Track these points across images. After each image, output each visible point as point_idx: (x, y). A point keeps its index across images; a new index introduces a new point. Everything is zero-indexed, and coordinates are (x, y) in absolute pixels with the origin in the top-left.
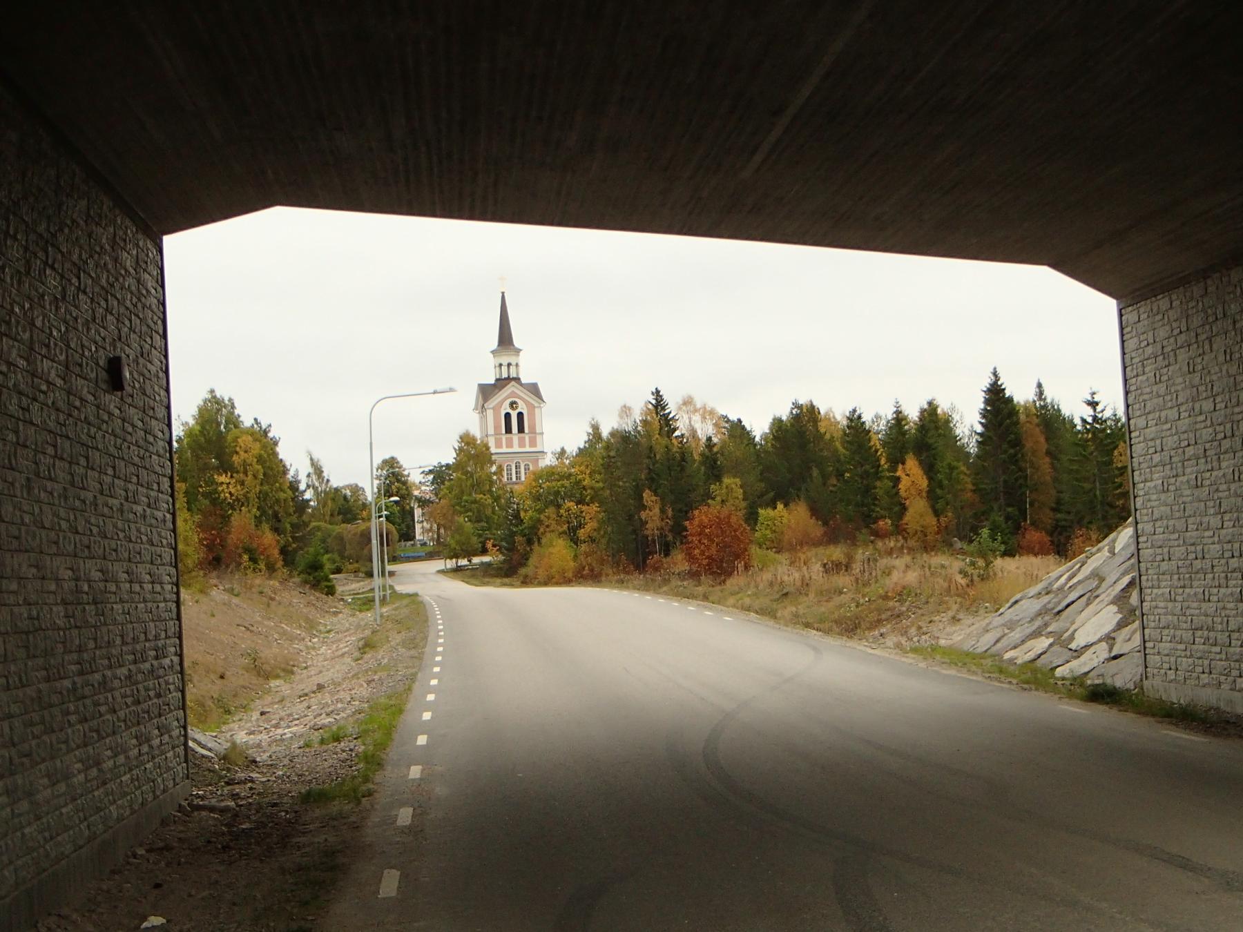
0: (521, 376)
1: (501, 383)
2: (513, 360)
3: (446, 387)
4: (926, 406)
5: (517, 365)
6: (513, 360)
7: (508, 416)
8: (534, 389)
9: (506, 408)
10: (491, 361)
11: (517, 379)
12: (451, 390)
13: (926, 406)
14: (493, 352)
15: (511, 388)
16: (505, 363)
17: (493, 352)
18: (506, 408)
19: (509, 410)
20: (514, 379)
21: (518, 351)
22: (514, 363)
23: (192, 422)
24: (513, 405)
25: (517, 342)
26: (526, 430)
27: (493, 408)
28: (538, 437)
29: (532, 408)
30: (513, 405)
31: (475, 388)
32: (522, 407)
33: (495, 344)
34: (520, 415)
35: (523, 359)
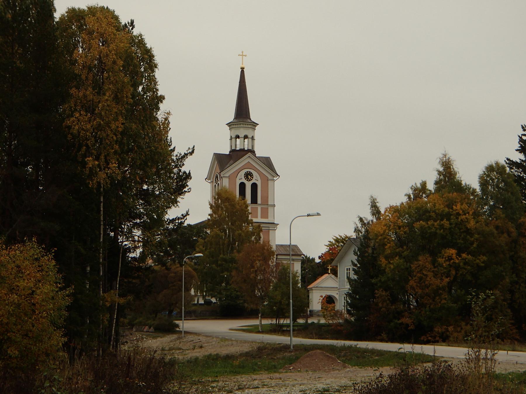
0: (256, 150)
1: (236, 154)
2: (249, 133)
3: (315, 212)
4: (419, 185)
5: (253, 138)
6: (249, 133)
7: (242, 186)
8: (267, 162)
9: (241, 178)
10: (227, 133)
11: (252, 152)
12: (318, 214)
13: (419, 185)
14: (229, 124)
15: (245, 160)
16: (242, 135)
17: (229, 124)
18: (241, 178)
19: (244, 180)
20: (249, 151)
21: (255, 125)
22: (250, 136)
23: (470, 176)
24: (248, 176)
25: (254, 117)
26: (259, 201)
27: (229, 177)
28: (270, 209)
29: (266, 181)
30: (248, 176)
31: (211, 156)
32: (257, 179)
33: (231, 116)
34: (254, 187)
35: (258, 133)
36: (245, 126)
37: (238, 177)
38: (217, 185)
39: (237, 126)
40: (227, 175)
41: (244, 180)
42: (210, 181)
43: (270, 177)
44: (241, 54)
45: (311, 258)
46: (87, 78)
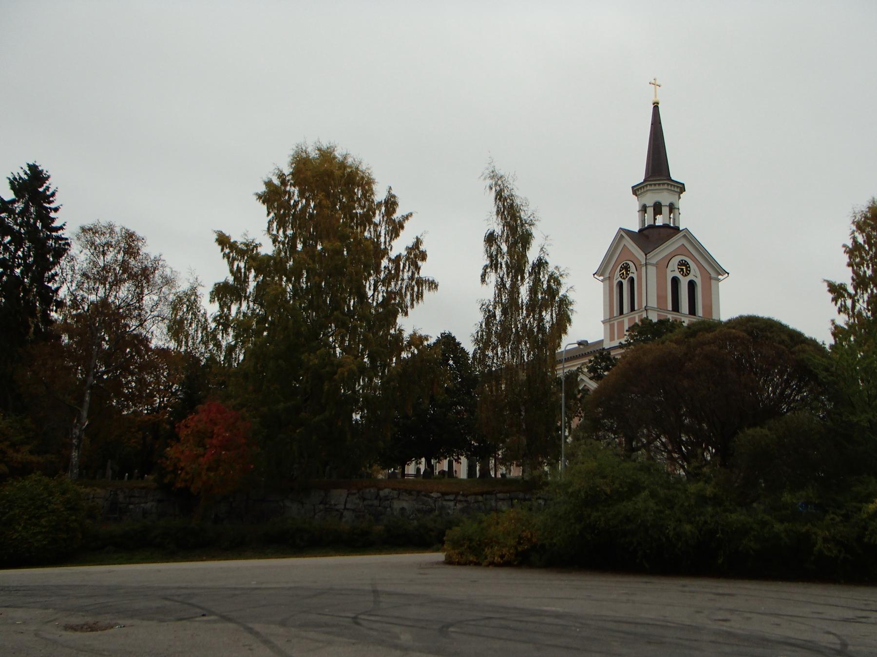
7: (675, 281)
9: (673, 270)
10: (634, 204)
18: (673, 270)
21: (681, 188)
24: (684, 267)
26: (636, 308)
27: (657, 265)
30: (684, 267)
33: (640, 177)
34: (692, 285)
35: (684, 202)
36: (653, 187)
38: (625, 283)
39: (657, 187)
40: (654, 261)
41: (620, 279)
42: (601, 278)
43: (713, 275)
44: (653, 82)
45: (255, 227)
46: (491, 391)
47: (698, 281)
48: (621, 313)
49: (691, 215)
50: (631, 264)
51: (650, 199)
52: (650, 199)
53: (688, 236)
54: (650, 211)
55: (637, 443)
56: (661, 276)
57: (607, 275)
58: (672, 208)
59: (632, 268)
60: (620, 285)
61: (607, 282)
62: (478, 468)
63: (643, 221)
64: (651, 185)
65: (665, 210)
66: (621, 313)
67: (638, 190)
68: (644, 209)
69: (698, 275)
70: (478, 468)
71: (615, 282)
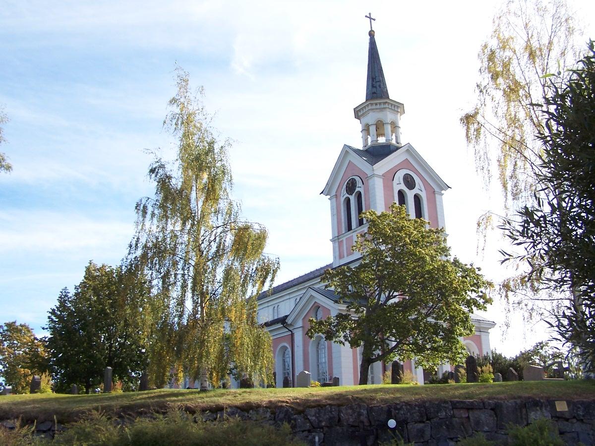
1: (376, 153)
7: (401, 194)
9: (399, 184)
10: (357, 125)
14: (359, 112)
21: (398, 107)
24: (409, 182)
30: (409, 182)
33: (361, 97)
34: (417, 198)
35: (403, 121)
36: (374, 107)
37: (342, 195)
38: (353, 199)
40: (381, 173)
43: (437, 189)
44: (369, 16)
47: (423, 195)
48: (349, 228)
49: (410, 131)
50: (357, 179)
51: (371, 118)
52: (371, 118)
53: (410, 150)
54: (373, 129)
55: (541, 221)
56: (388, 187)
57: (334, 193)
58: (395, 126)
59: (359, 183)
60: (348, 201)
61: (334, 199)
62: (55, 417)
63: (366, 140)
64: (372, 104)
65: (388, 128)
66: (349, 228)
67: (360, 111)
68: (366, 129)
69: (423, 188)
70: (55, 417)
71: (342, 199)
